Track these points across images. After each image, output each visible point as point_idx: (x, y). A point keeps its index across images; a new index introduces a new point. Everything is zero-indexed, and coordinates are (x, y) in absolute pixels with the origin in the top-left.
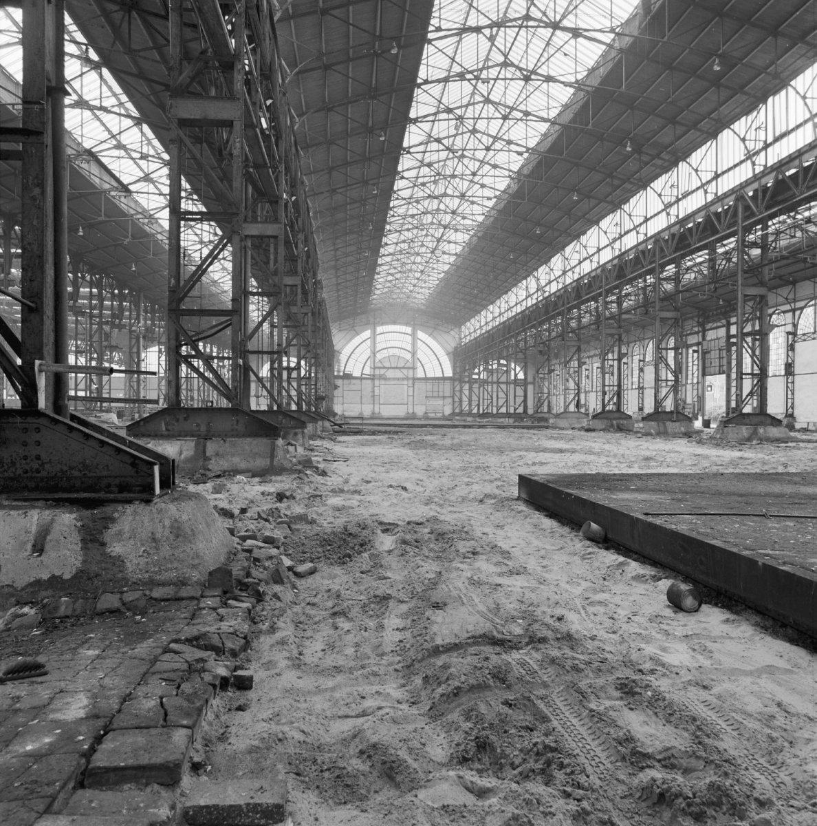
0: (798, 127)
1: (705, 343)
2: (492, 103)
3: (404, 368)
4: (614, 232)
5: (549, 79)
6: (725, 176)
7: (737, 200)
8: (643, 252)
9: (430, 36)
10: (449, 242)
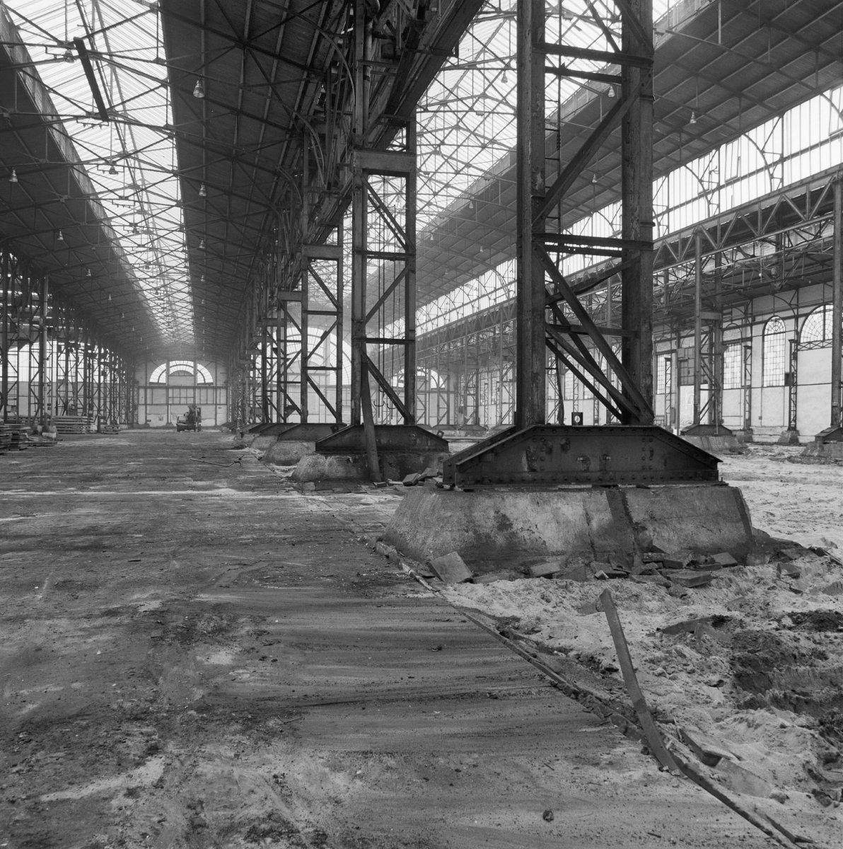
1: (680, 351)
4: (445, 308)
6: (795, 159)
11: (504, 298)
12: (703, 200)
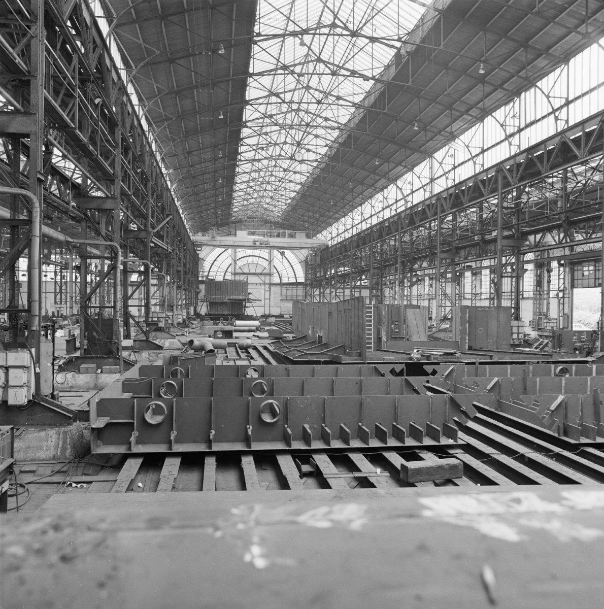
0: (543, 118)
2: (324, 62)
3: (261, 274)
5: (354, 73)
6: (490, 151)
7: (497, 172)
8: (428, 206)
9: (256, 39)
10: (295, 173)
11: (403, 208)
12: (471, 162)
